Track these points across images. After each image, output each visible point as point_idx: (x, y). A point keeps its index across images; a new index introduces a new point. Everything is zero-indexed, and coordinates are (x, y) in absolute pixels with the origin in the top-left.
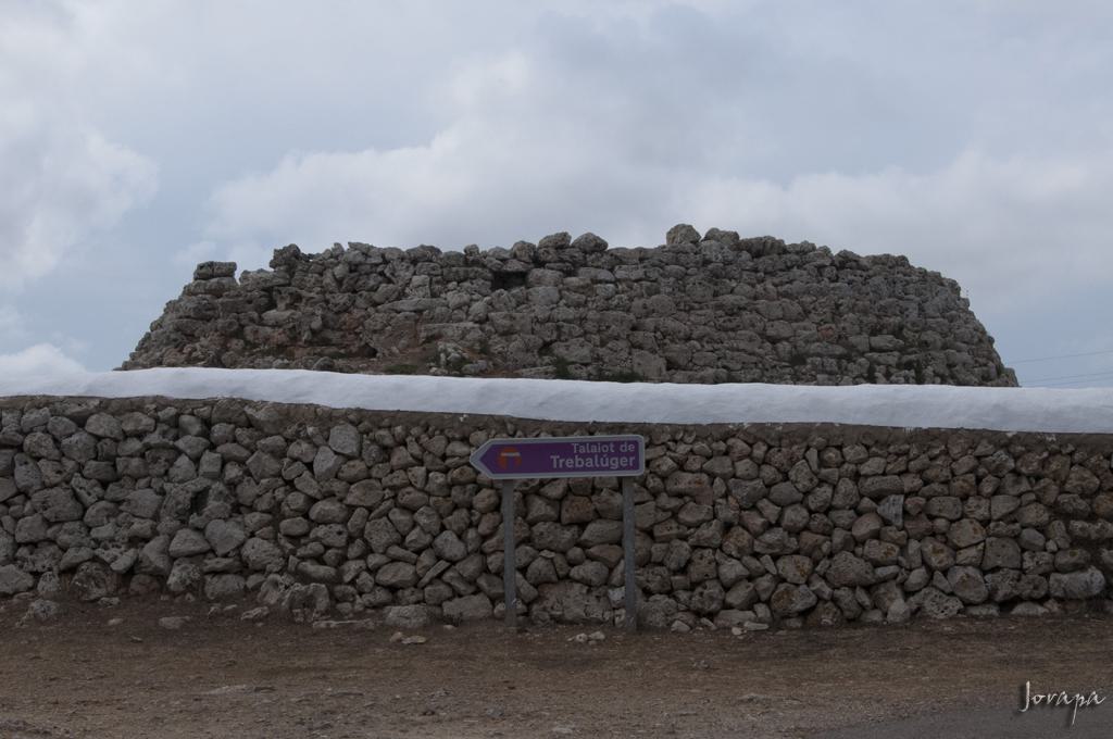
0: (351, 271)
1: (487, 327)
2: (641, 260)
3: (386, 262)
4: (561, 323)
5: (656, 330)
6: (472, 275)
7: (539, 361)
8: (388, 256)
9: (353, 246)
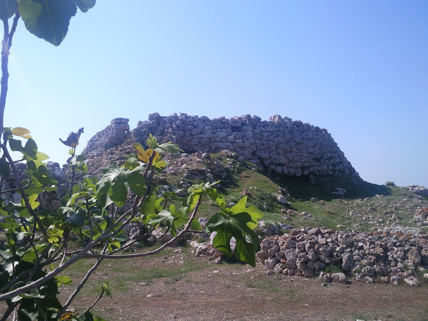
0: (182, 123)
1: (234, 144)
2: (272, 125)
3: (194, 121)
4: (257, 145)
5: (282, 148)
6: (225, 127)
7: (253, 158)
8: (195, 119)
9: (182, 114)
